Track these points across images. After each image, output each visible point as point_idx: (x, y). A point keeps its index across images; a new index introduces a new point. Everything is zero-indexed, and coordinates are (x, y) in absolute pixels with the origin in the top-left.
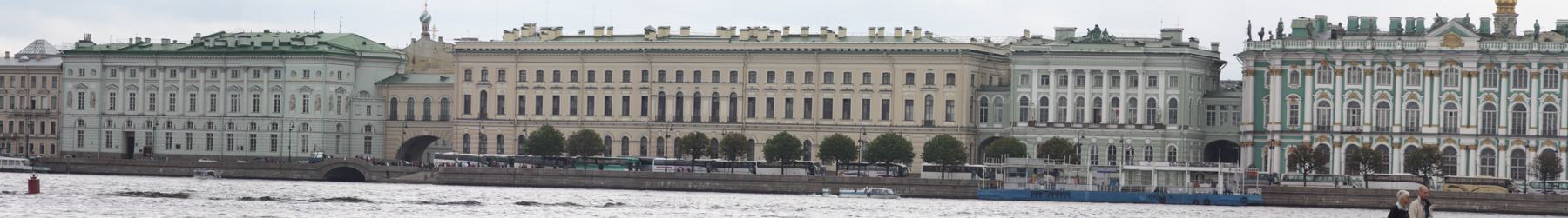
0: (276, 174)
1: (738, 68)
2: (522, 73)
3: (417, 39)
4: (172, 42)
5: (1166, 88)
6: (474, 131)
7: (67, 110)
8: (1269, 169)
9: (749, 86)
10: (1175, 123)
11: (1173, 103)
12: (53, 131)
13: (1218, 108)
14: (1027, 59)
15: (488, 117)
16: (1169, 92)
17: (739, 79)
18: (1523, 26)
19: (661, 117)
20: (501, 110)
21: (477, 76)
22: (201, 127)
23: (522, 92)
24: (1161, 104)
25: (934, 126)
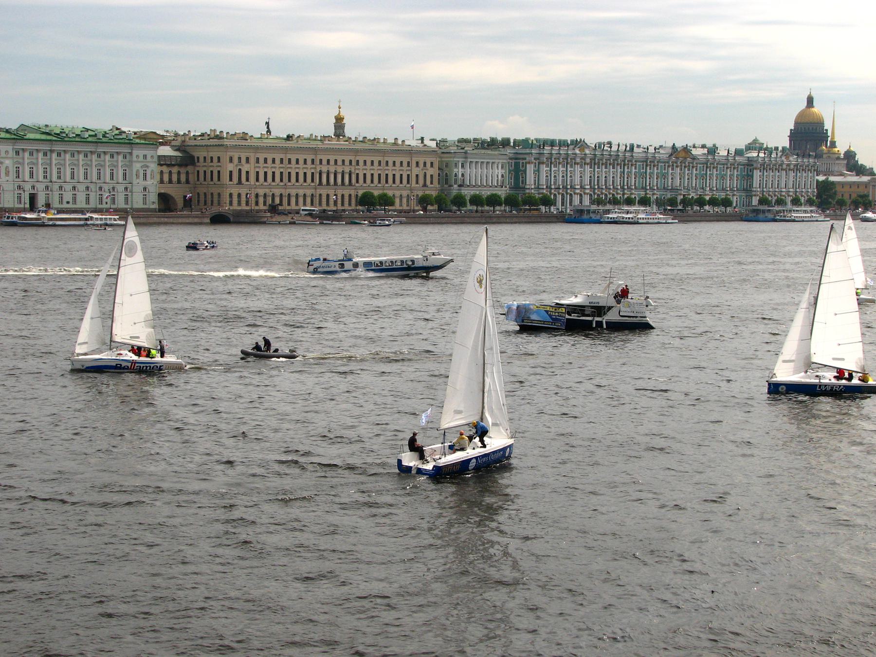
0: (699, 219)
2: (258, 159)
3: (388, 141)
4: (382, 141)
6: (235, 191)
7: (135, 181)
8: (129, 202)
9: (357, 167)
18: (274, 134)
19: (320, 183)
20: (247, 180)
21: (236, 160)
23: (257, 170)
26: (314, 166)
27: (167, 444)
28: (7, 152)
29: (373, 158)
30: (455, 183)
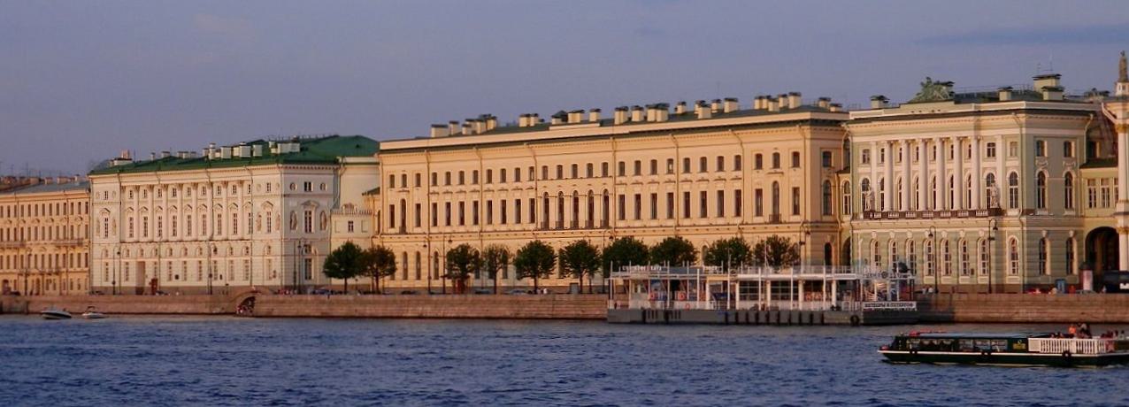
1: (422, 169)
5: (1005, 159)
9: (619, 179)
10: (1016, 206)
11: (1013, 179)
12: (86, 266)
13: (1098, 182)
14: (928, 125)
15: (407, 231)
16: (1008, 164)
17: (610, 173)
22: (239, 253)
24: (1001, 181)
25: (781, 223)
26: (533, 184)
27: (45, 339)
28: (322, 186)
29: (654, 155)
30: (1014, 205)
